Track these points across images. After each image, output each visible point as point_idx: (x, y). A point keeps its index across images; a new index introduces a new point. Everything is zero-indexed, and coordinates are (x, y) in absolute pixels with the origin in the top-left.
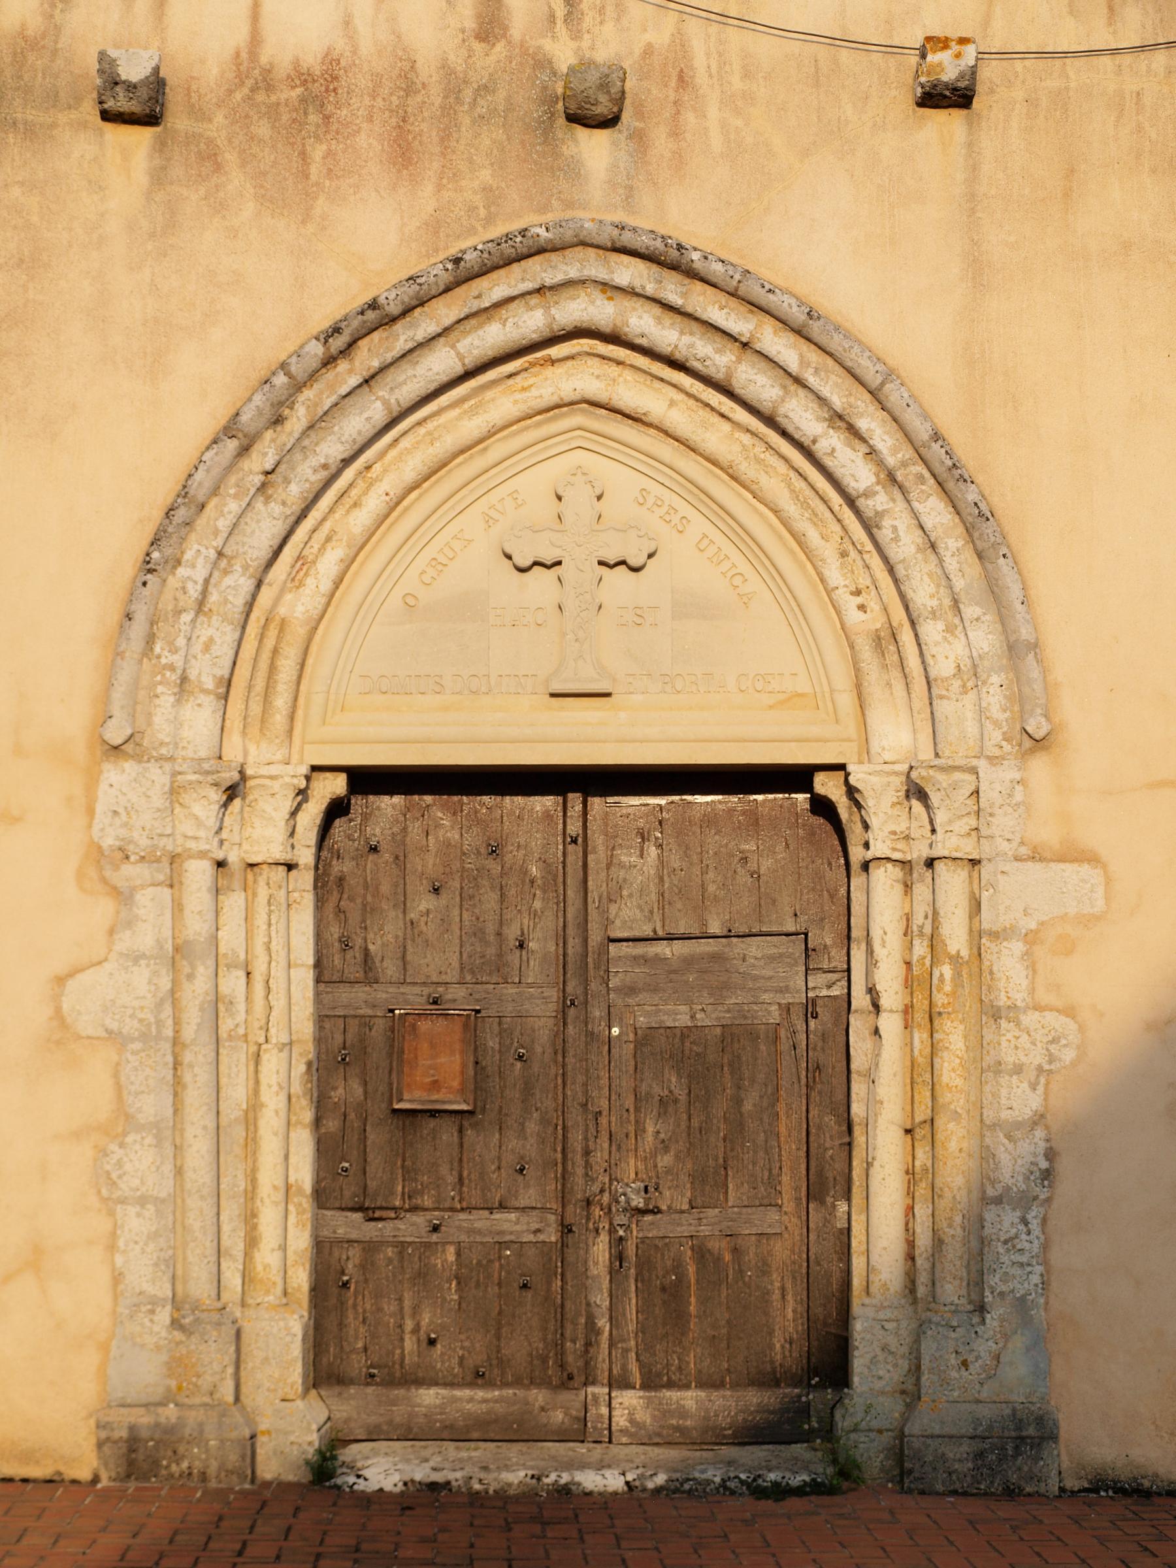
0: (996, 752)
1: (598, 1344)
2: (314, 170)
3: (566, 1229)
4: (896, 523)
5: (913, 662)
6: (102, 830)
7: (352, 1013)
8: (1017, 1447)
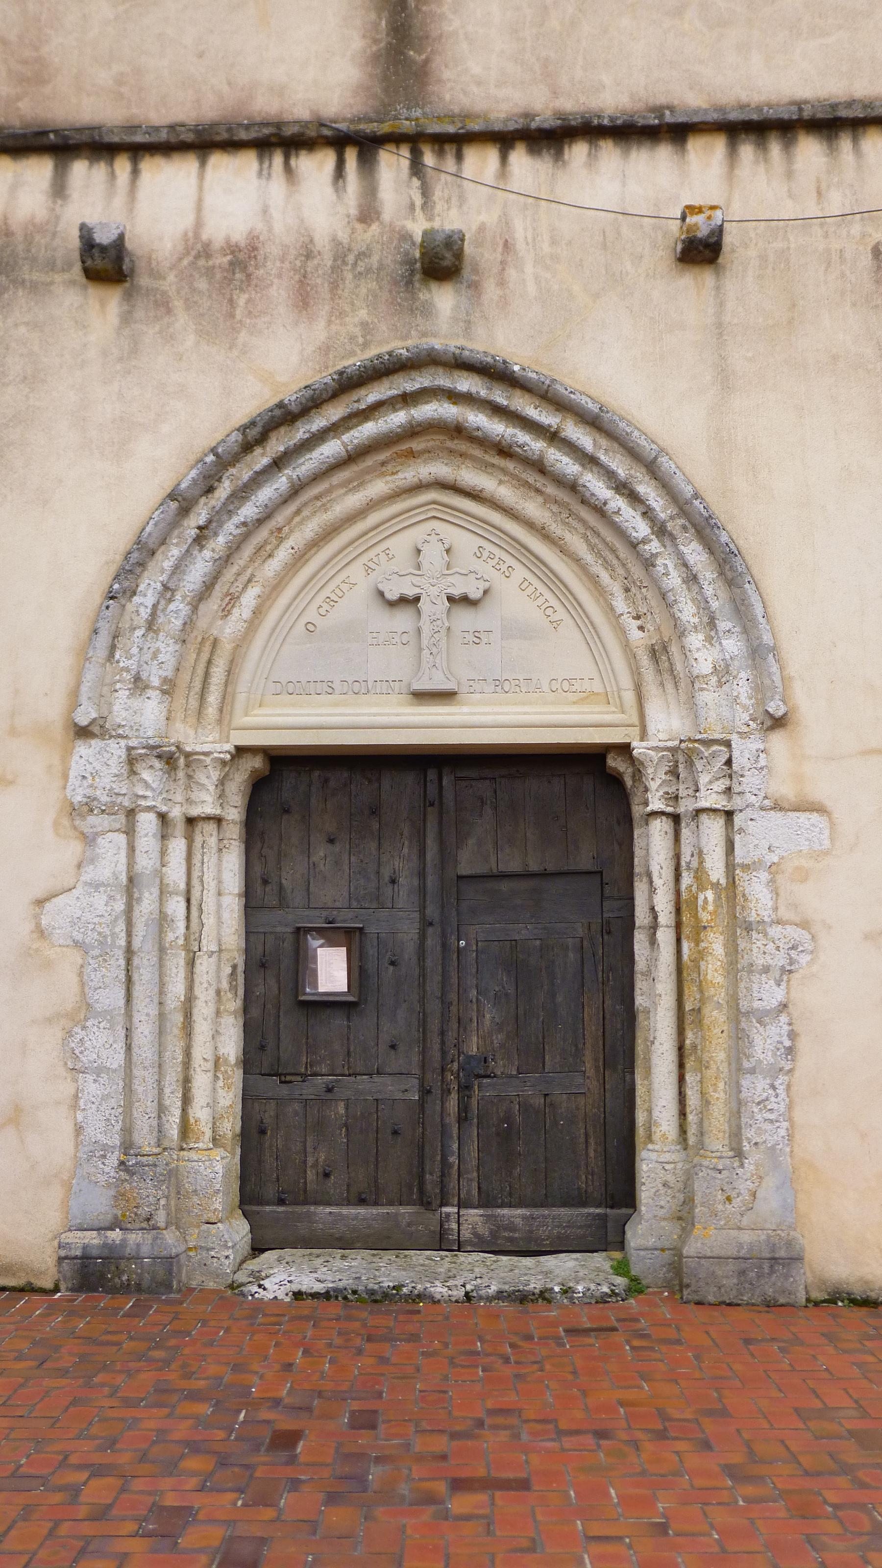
0: (746, 729)
1: (450, 1174)
2: (239, 313)
3: (425, 1092)
5: (679, 667)
6: (74, 790)
8: (771, 1267)
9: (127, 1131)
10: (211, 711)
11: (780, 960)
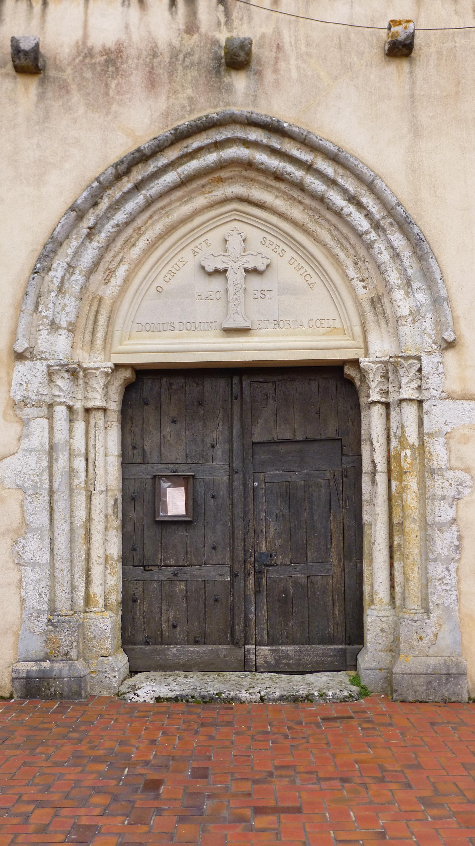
0: (430, 349)
2: (111, 92)
3: (234, 575)
4: (380, 245)
5: (388, 311)
6: (15, 392)
7: (137, 477)
9: (52, 601)
10: (99, 343)
11: (452, 492)
